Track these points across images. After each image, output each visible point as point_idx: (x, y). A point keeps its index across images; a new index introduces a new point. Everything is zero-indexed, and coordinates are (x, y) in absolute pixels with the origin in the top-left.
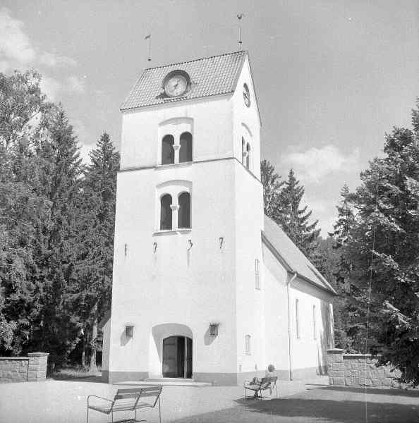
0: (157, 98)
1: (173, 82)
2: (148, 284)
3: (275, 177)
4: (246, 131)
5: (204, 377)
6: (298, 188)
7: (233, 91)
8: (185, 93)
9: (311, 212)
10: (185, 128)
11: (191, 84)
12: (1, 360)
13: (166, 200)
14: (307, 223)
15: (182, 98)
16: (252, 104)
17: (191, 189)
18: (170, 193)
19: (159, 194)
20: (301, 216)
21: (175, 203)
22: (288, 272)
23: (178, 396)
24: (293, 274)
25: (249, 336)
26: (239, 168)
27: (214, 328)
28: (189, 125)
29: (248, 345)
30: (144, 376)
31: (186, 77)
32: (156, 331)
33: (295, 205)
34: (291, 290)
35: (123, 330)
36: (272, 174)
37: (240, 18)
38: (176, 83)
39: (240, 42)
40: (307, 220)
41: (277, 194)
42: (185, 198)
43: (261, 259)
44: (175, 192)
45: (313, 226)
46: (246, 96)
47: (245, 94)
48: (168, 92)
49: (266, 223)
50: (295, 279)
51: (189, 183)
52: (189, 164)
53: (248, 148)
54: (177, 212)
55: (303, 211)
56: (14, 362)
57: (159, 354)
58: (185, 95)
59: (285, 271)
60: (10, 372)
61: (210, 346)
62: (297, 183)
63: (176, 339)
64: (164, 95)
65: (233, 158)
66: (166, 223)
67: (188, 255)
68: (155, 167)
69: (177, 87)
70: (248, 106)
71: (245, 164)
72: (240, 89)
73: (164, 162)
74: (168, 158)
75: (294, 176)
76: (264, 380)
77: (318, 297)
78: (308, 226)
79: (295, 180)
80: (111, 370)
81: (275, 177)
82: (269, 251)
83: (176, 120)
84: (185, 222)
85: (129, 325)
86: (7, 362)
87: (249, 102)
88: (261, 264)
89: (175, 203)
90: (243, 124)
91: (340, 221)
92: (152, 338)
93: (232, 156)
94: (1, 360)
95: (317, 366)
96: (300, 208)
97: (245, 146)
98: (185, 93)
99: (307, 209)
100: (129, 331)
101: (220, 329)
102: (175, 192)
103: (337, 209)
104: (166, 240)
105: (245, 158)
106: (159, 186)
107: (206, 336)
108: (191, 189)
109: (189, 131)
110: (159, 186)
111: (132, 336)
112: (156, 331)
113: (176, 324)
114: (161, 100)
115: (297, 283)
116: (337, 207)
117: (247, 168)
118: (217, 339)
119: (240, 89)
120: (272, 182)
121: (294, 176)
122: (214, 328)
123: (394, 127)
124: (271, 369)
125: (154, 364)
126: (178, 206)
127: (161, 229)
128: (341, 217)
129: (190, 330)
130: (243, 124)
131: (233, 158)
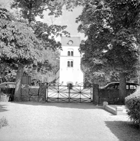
42: (72, 62)
44: (70, 61)
48: (69, 44)
51: (73, 60)
66: (69, 66)
68: (67, 56)
69: (70, 43)
84: (72, 66)
101: (64, 82)
102: (70, 61)
114: (67, 45)
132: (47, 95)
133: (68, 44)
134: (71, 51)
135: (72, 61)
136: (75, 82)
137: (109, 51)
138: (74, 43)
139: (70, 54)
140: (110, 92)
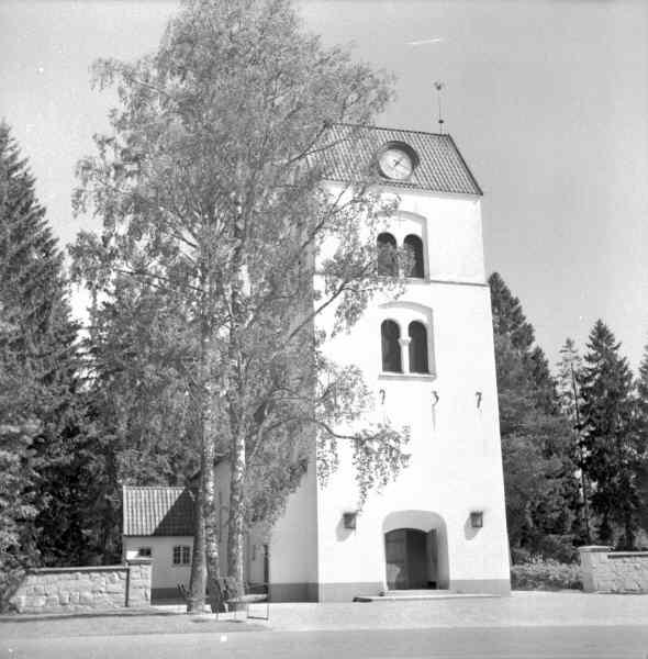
5: (466, 587)
18: (382, 321)
21: (405, 337)
23: (417, 609)
31: (408, 153)
35: (340, 517)
37: (439, 88)
39: (441, 122)
42: (418, 330)
44: (404, 319)
51: (429, 311)
56: (94, 574)
60: (88, 594)
61: (473, 540)
63: (404, 534)
67: (433, 410)
84: (421, 364)
85: (477, 509)
86: (79, 574)
89: (405, 337)
102: (404, 319)
107: (466, 527)
109: (420, 234)
111: (354, 528)
113: (402, 513)
118: (481, 531)
123: (75, 216)
126: (410, 339)
135: (423, 318)
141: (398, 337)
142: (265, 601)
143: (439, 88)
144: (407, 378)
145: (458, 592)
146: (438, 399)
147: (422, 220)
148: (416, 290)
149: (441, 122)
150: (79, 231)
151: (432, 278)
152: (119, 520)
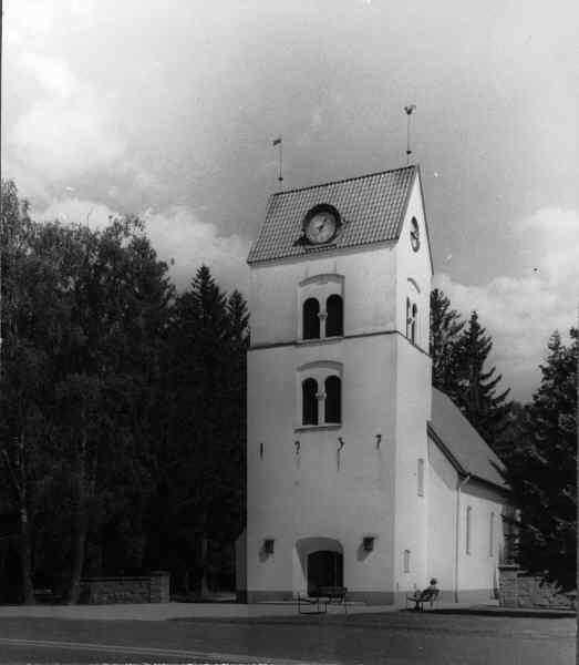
0: (295, 245)
1: (317, 222)
2: (296, 486)
3: (449, 318)
4: (413, 287)
6: (482, 340)
7: (397, 238)
8: (334, 237)
9: (499, 378)
10: (333, 288)
11: (341, 224)
12: (2, 626)
13: (309, 386)
14: (493, 393)
15: (329, 246)
16: (421, 247)
17: (341, 374)
19: (300, 378)
20: (485, 383)
21: (322, 390)
22: (459, 474)
24: (465, 476)
25: (408, 552)
26: (403, 343)
27: (368, 544)
28: (340, 285)
29: (407, 562)
30: (287, 597)
32: (302, 546)
33: (479, 366)
34: (464, 496)
36: (448, 312)
37: (409, 112)
38: (320, 224)
40: (491, 390)
41: (452, 343)
42: (334, 384)
43: (426, 458)
44: (320, 376)
45: (502, 398)
46: (414, 235)
47: (412, 234)
48: (312, 238)
49: (434, 394)
50: (469, 482)
51: (339, 365)
52: (340, 340)
53: (414, 311)
54: (324, 403)
55: (490, 375)
57: (303, 566)
58: (334, 242)
59: (456, 473)
62: (482, 332)
64: (304, 241)
65: (395, 332)
66: (310, 416)
68: (294, 343)
69: (321, 229)
70: (416, 250)
71: (410, 337)
72: (407, 227)
73: (305, 337)
74: (311, 331)
75: (478, 321)
76: (426, 592)
77: (497, 501)
78: (494, 397)
79: (479, 327)
80: (250, 589)
81: (449, 318)
82: (437, 448)
83: (322, 278)
84: (334, 415)
87: (418, 244)
88: (427, 465)
89: (322, 390)
90: (410, 280)
91: (543, 387)
92: (295, 551)
93: (393, 329)
94: (2, 626)
95: (492, 587)
96: (485, 371)
97: (411, 310)
98: (334, 237)
99: (495, 372)
100: (269, 546)
101: (376, 544)
102: (320, 376)
103: (540, 370)
104: (308, 438)
105: (410, 326)
106: (302, 369)
108: (341, 374)
109: (339, 293)
110: (302, 369)
111: (272, 552)
112: (302, 546)
114: (300, 249)
115: (472, 488)
116: (541, 366)
117: (412, 342)
118: (372, 554)
119: (407, 227)
120: (447, 324)
121: (478, 321)
122: (368, 544)
124: (433, 582)
125: (299, 584)
126: (325, 395)
127: (304, 424)
128: (545, 382)
129: (340, 546)
130: (410, 280)
131: (395, 332)
132: (112, 649)
133: (304, 241)
134: (322, 293)
135: (336, 373)
136: (360, 542)
137: (520, 535)
138: (345, 231)
139: (323, 324)
140: (87, 260)
141: (316, 391)
142: (236, 602)
143: (409, 112)
144: (323, 428)
145: (285, 600)
146: (342, 443)
147: (339, 278)
148: (330, 350)
149: (409, 152)
150: (207, 265)
151: (346, 334)
152: (474, 420)
